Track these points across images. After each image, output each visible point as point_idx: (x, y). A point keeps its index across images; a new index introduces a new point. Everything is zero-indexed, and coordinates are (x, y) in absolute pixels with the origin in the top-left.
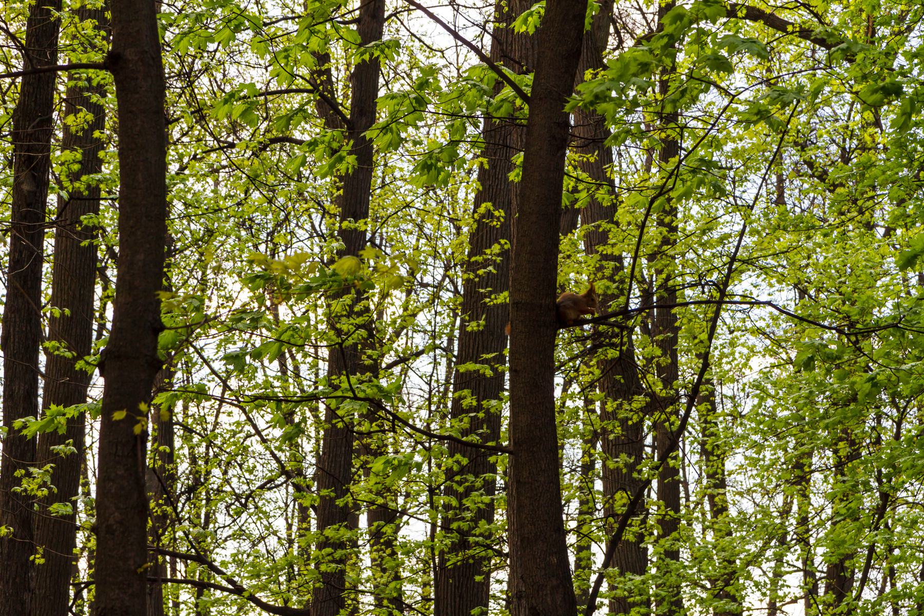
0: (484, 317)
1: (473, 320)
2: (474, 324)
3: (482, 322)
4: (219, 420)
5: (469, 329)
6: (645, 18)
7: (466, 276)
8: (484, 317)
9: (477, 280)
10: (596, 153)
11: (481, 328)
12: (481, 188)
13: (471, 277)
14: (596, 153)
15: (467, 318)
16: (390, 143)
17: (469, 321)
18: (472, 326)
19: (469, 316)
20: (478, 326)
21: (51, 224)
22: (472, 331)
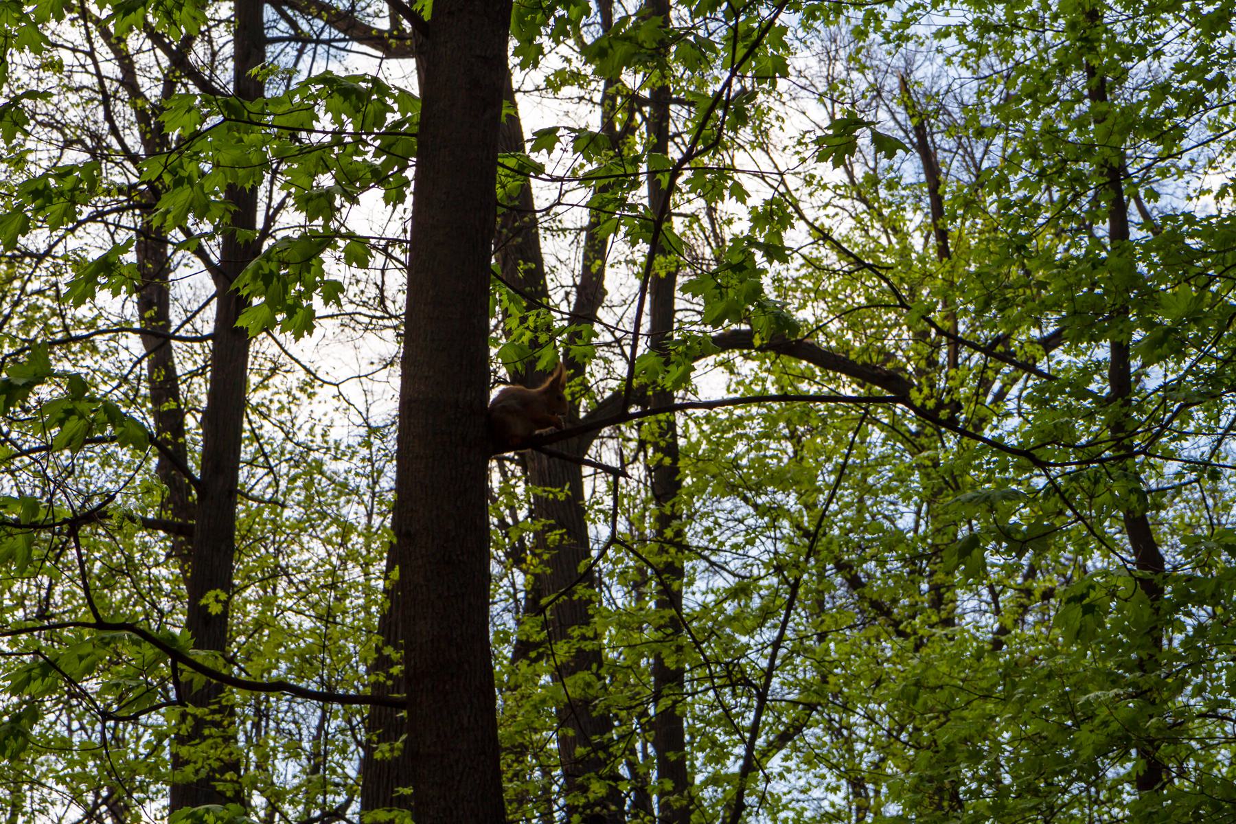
0: (404, 737)
1: (384, 741)
2: (385, 747)
3: (399, 744)
4: (532, 88)
5: (378, 755)
6: (895, 119)
7: (373, 678)
8: (404, 737)
9: (390, 683)
10: (567, 487)
11: (396, 754)
12: (395, 541)
13: (382, 679)
14: (567, 487)
15: (375, 738)
16: (191, 205)
17: (378, 742)
18: (383, 751)
19: (378, 736)
20: (392, 750)
21: (186, 521)
22: (383, 760)
